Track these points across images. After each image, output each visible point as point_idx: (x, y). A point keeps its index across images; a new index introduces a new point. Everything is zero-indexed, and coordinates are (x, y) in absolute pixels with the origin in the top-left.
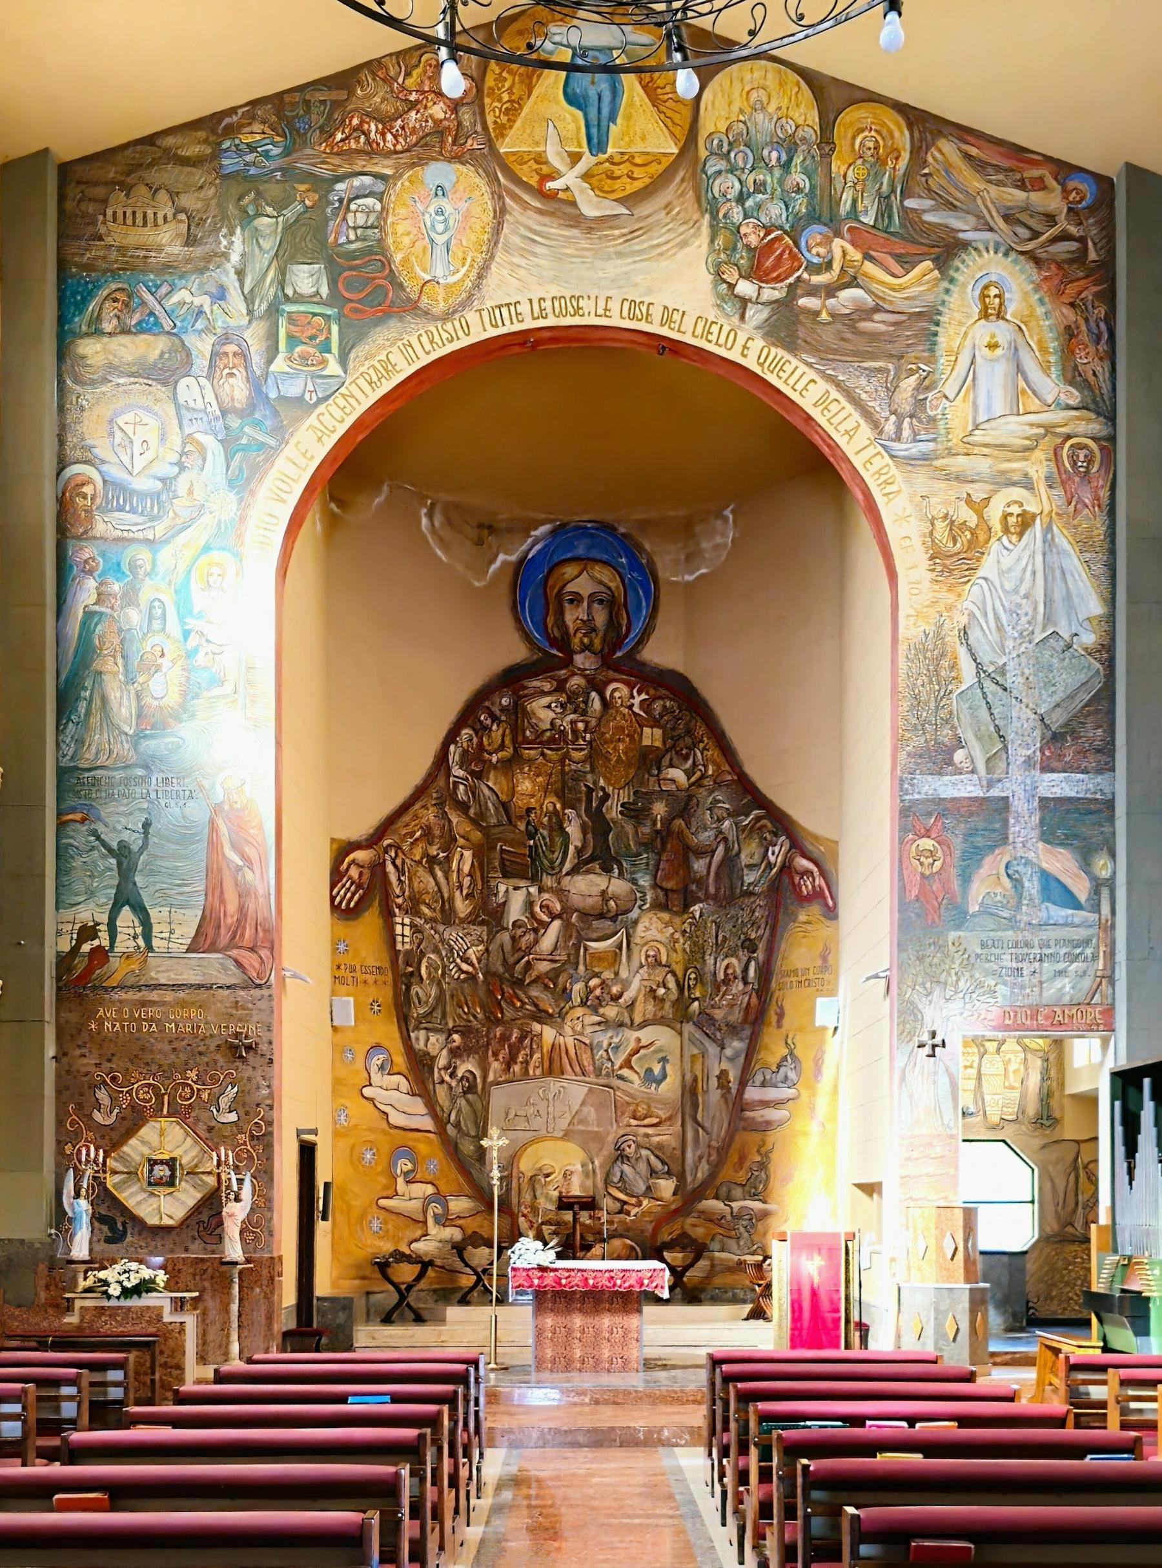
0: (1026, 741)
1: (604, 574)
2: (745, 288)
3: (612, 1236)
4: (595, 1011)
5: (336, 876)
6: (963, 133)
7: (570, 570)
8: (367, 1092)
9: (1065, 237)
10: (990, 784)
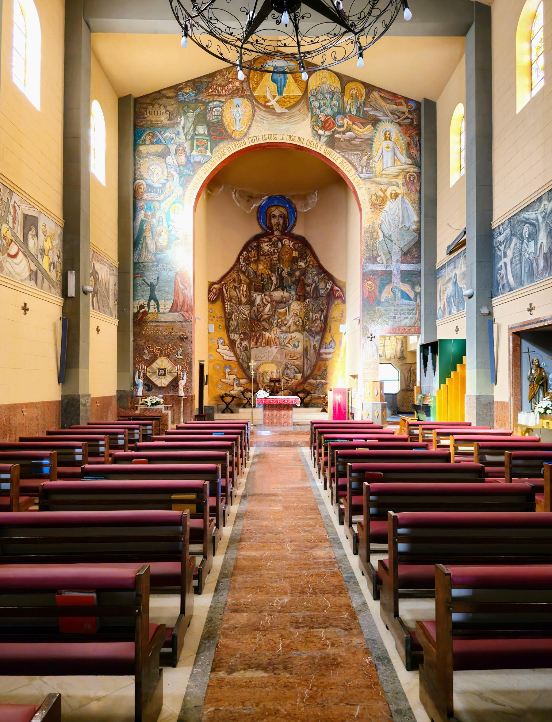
0: (397, 255)
1: (282, 210)
2: (321, 132)
3: (284, 390)
4: (280, 328)
5: (210, 291)
6: (380, 90)
7: (273, 209)
8: (218, 350)
9: (407, 118)
10: (387, 267)
